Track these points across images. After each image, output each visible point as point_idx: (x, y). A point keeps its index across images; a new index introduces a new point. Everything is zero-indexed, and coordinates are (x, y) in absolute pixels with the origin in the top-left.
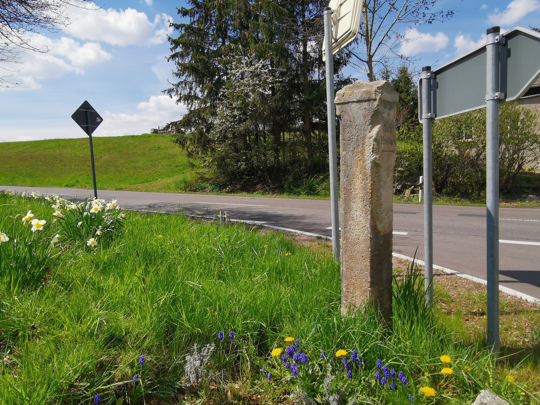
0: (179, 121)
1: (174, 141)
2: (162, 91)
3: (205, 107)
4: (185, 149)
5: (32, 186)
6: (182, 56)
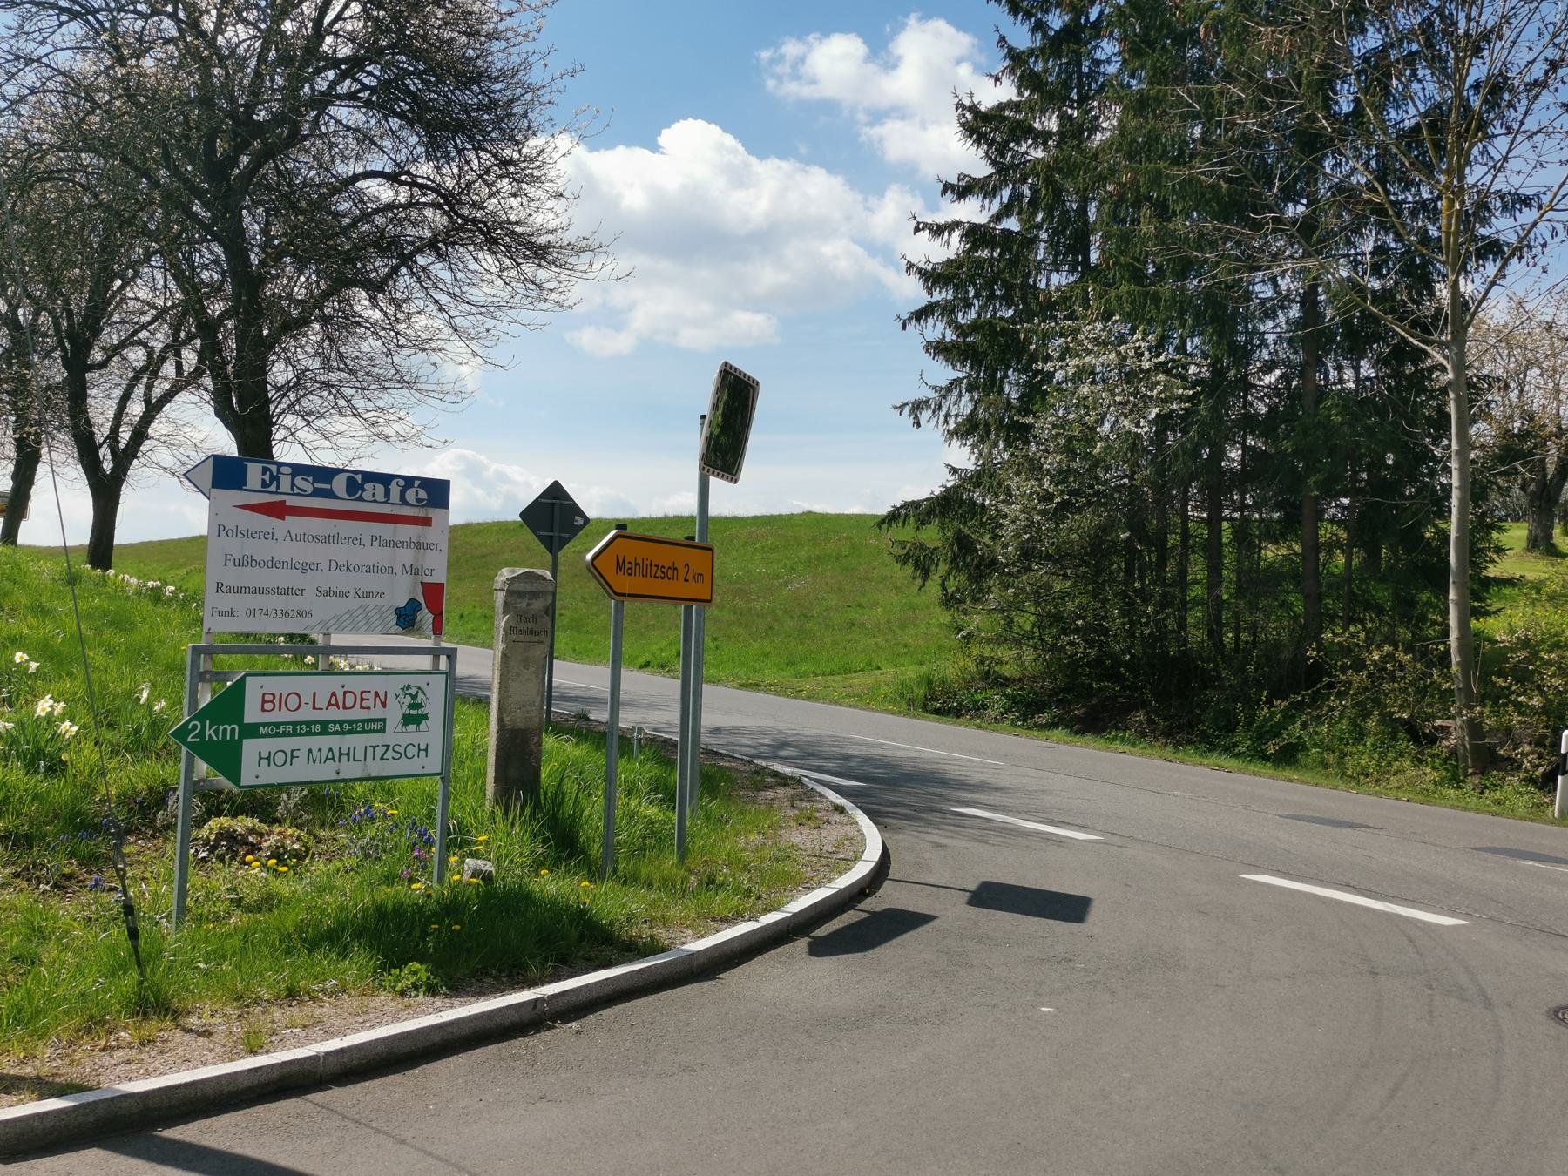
0: (927, 499)
1: (898, 559)
2: (895, 407)
3: (1416, 371)
6: (947, 310)
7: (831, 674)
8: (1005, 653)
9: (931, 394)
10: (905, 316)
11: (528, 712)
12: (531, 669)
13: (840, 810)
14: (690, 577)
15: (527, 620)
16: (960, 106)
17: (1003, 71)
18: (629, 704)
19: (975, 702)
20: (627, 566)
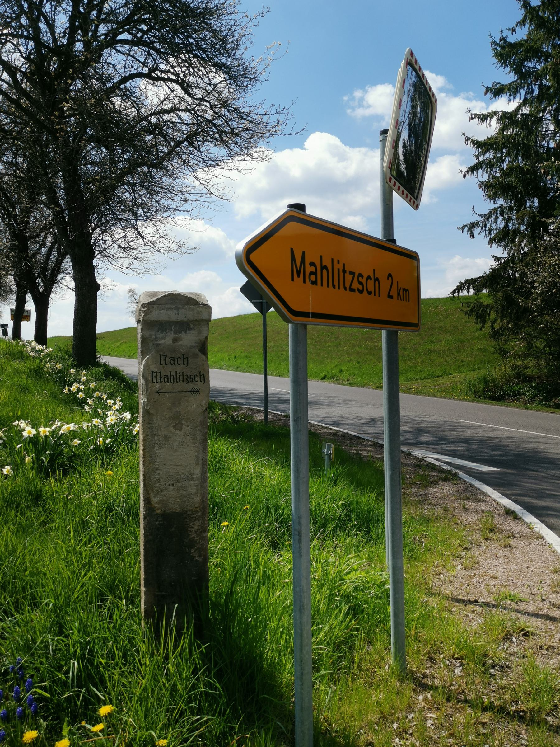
0: (480, 277)
2: (459, 228)
4: (488, 325)
5: (280, 376)
6: (490, 165)
7: (425, 378)
8: (531, 363)
9: (479, 219)
10: (465, 170)
11: (184, 488)
12: (185, 429)
13: (509, 513)
14: (394, 293)
15: (174, 361)
16: (494, 43)
17: (517, 25)
18: (317, 403)
19: (514, 392)
20: (309, 269)
